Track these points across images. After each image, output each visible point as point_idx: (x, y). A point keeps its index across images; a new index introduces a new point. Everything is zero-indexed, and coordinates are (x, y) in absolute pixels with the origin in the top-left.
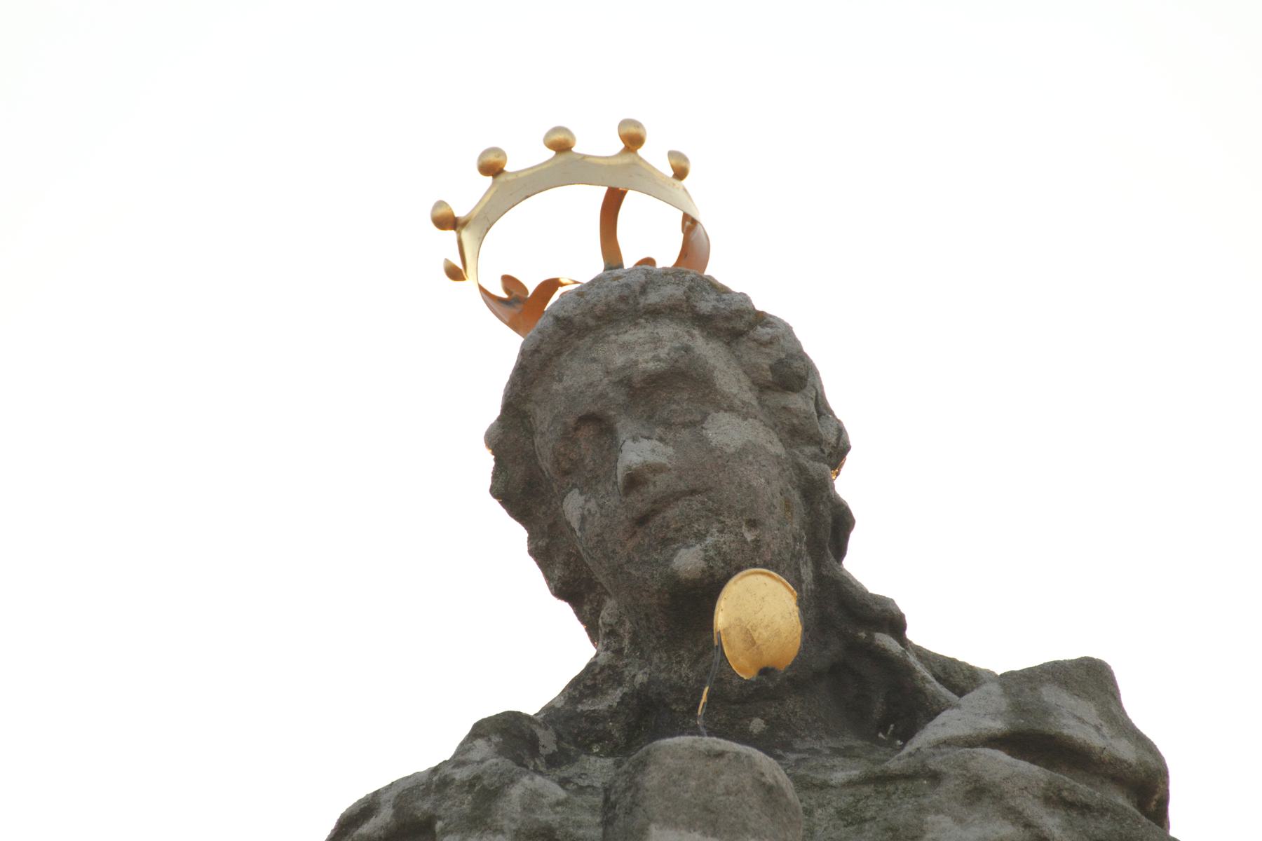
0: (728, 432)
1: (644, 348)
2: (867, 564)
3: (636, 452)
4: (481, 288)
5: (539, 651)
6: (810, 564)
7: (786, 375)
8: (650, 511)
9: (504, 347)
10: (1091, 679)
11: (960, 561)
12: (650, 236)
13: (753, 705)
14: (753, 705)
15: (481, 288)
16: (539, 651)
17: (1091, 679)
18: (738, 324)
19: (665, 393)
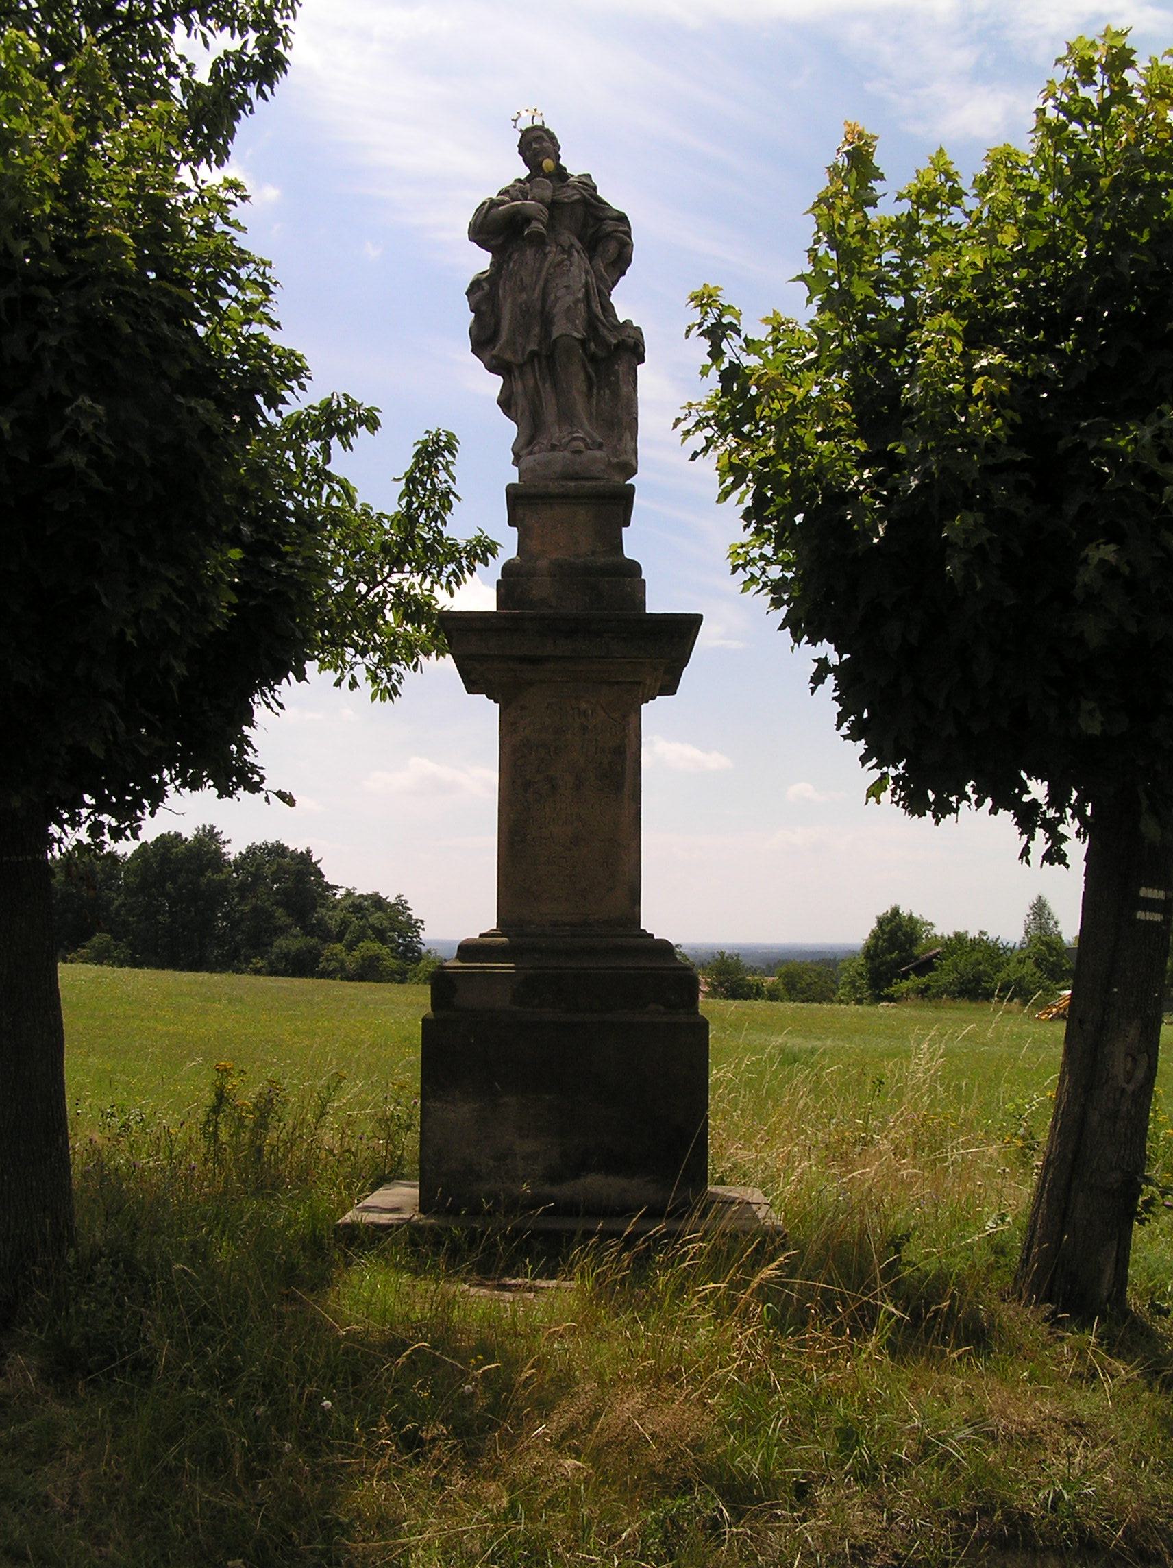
0: (545, 144)
1: (375, 918)
2: (562, 162)
3: (535, 146)
4: (793, 280)
5: (524, 172)
6: (1076, 849)
7: (552, 138)
8: (536, 154)
9: (520, 135)
10: (589, 176)
11: (573, 164)
12: (538, 122)
13: (548, 176)
14: (548, 176)
15: (793, 280)
16: (524, 172)
17: (589, 176)
18: (547, 131)
19: (539, 139)
